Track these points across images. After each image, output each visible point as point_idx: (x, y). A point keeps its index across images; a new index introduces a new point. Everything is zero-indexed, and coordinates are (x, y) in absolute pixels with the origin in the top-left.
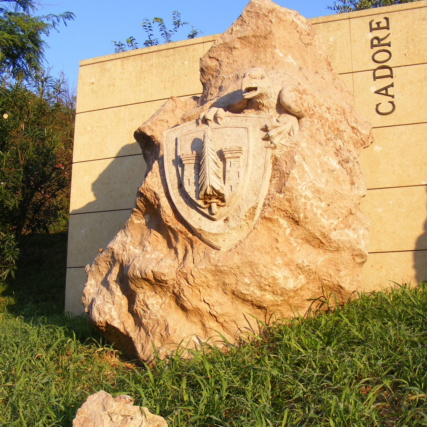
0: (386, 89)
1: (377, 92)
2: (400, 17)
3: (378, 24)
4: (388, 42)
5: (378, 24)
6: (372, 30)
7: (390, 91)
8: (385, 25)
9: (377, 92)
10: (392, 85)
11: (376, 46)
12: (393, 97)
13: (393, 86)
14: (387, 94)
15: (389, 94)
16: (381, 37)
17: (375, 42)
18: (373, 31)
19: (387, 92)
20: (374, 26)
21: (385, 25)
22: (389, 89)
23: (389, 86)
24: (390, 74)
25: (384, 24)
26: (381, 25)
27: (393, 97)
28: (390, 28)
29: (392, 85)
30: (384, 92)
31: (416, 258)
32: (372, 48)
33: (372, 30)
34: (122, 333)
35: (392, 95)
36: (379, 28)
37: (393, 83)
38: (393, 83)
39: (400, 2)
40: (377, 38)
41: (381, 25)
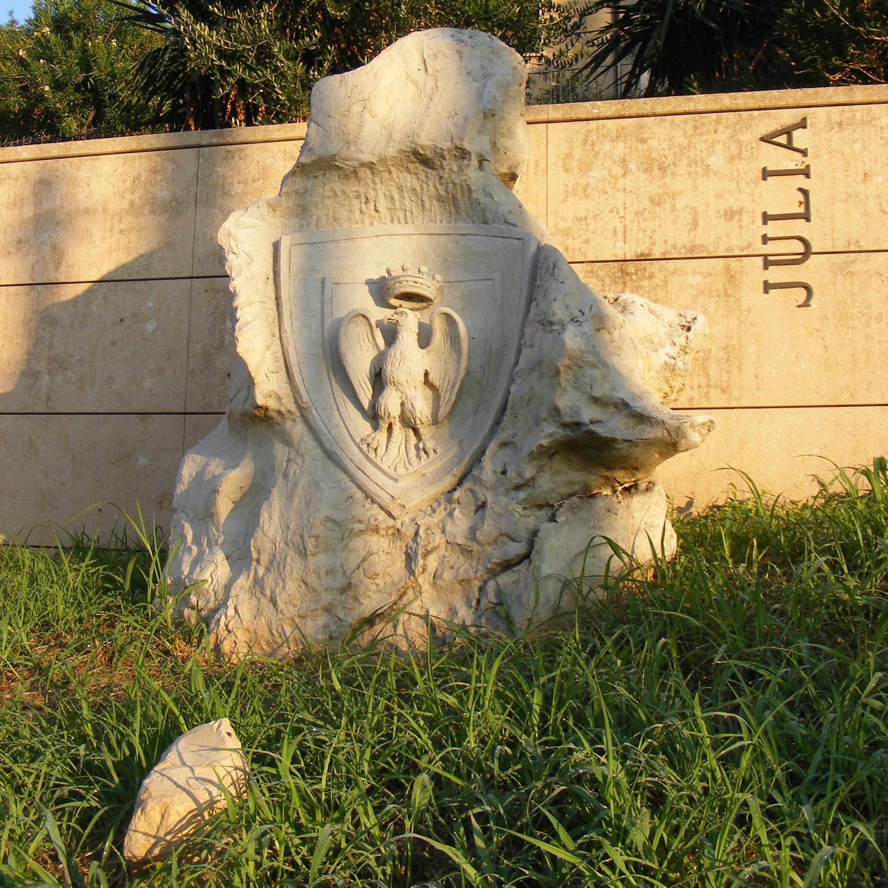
0: (788, 131)
1: (767, 139)
7: (800, 138)
9: (767, 139)
12: (804, 153)
13: (805, 127)
14: (789, 146)
15: (795, 145)
19: (790, 139)
22: (797, 134)
27: (804, 153)
29: (803, 124)
30: (783, 139)
37: (804, 119)
38: (804, 119)
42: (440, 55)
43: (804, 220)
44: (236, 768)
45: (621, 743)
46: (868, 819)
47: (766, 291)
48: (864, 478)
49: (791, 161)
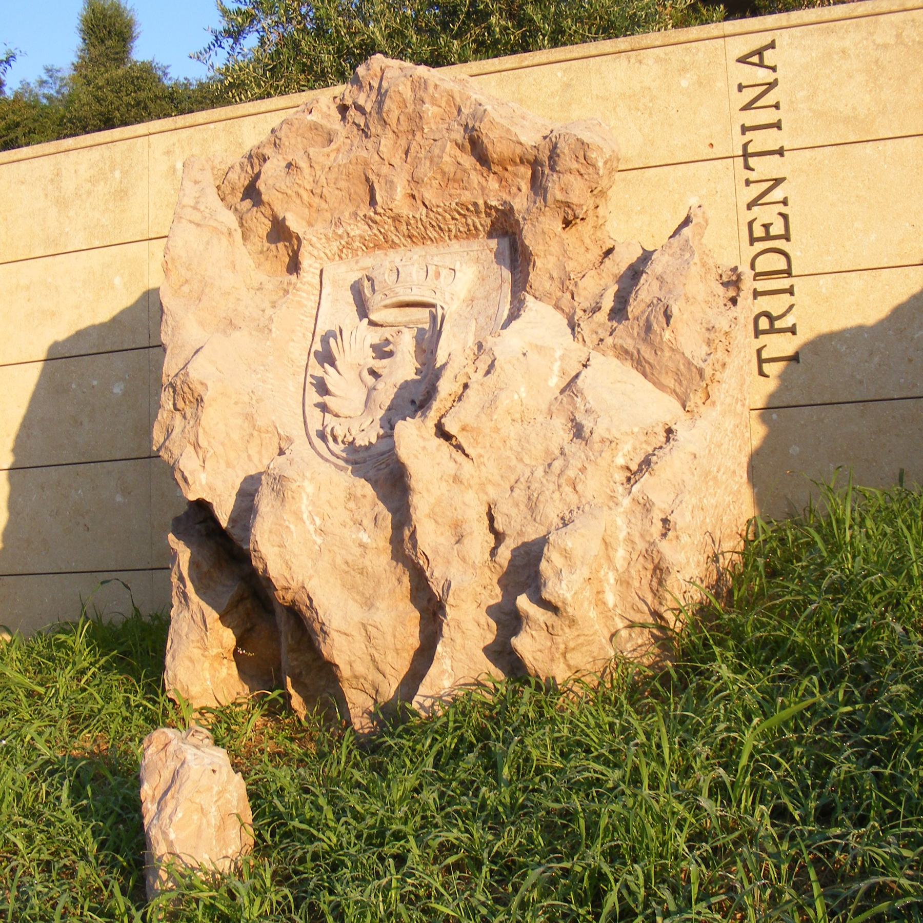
0: (759, 52)
1: (742, 60)
2: (791, 37)
3: (766, 227)
4: (790, 325)
5: (766, 227)
6: (753, 240)
7: (769, 57)
8: (782, 232)
9: (742, 60)
10: (772, 45)
11: (765, 332)
12: (774, 69)
13: (773, 47)
14: (761, 65)
15: (766, 63)
16: (775, 314)
17: (764, 323)
18: (761, 336)
19: (761, 59)
20: (759, 232)
21: (782, 232)
22: (767, 54)
23: (767, 47)
24: (786, 267)
25: (777, 228)
26: (774, 231)
27: (774, 69)
28: (793, 237)
29: (772, 45)
30: (755, 59)
31: (10, 479)
32: (751, 244)
33: (753, 240)
34: (143, 824)
35: (772, 65)
36: (768, 237)
37: (773, 41)
38: (773, 41)
39: (787, 9)
40: (767, 315)
41: (774, 231)
42: (548, 139)
43: (776, 129)
44: (632, 625)
45: (368, 36)
46: (822, 886)
47: (778, 103)
48: (539, 653)
49: (763, 75)
